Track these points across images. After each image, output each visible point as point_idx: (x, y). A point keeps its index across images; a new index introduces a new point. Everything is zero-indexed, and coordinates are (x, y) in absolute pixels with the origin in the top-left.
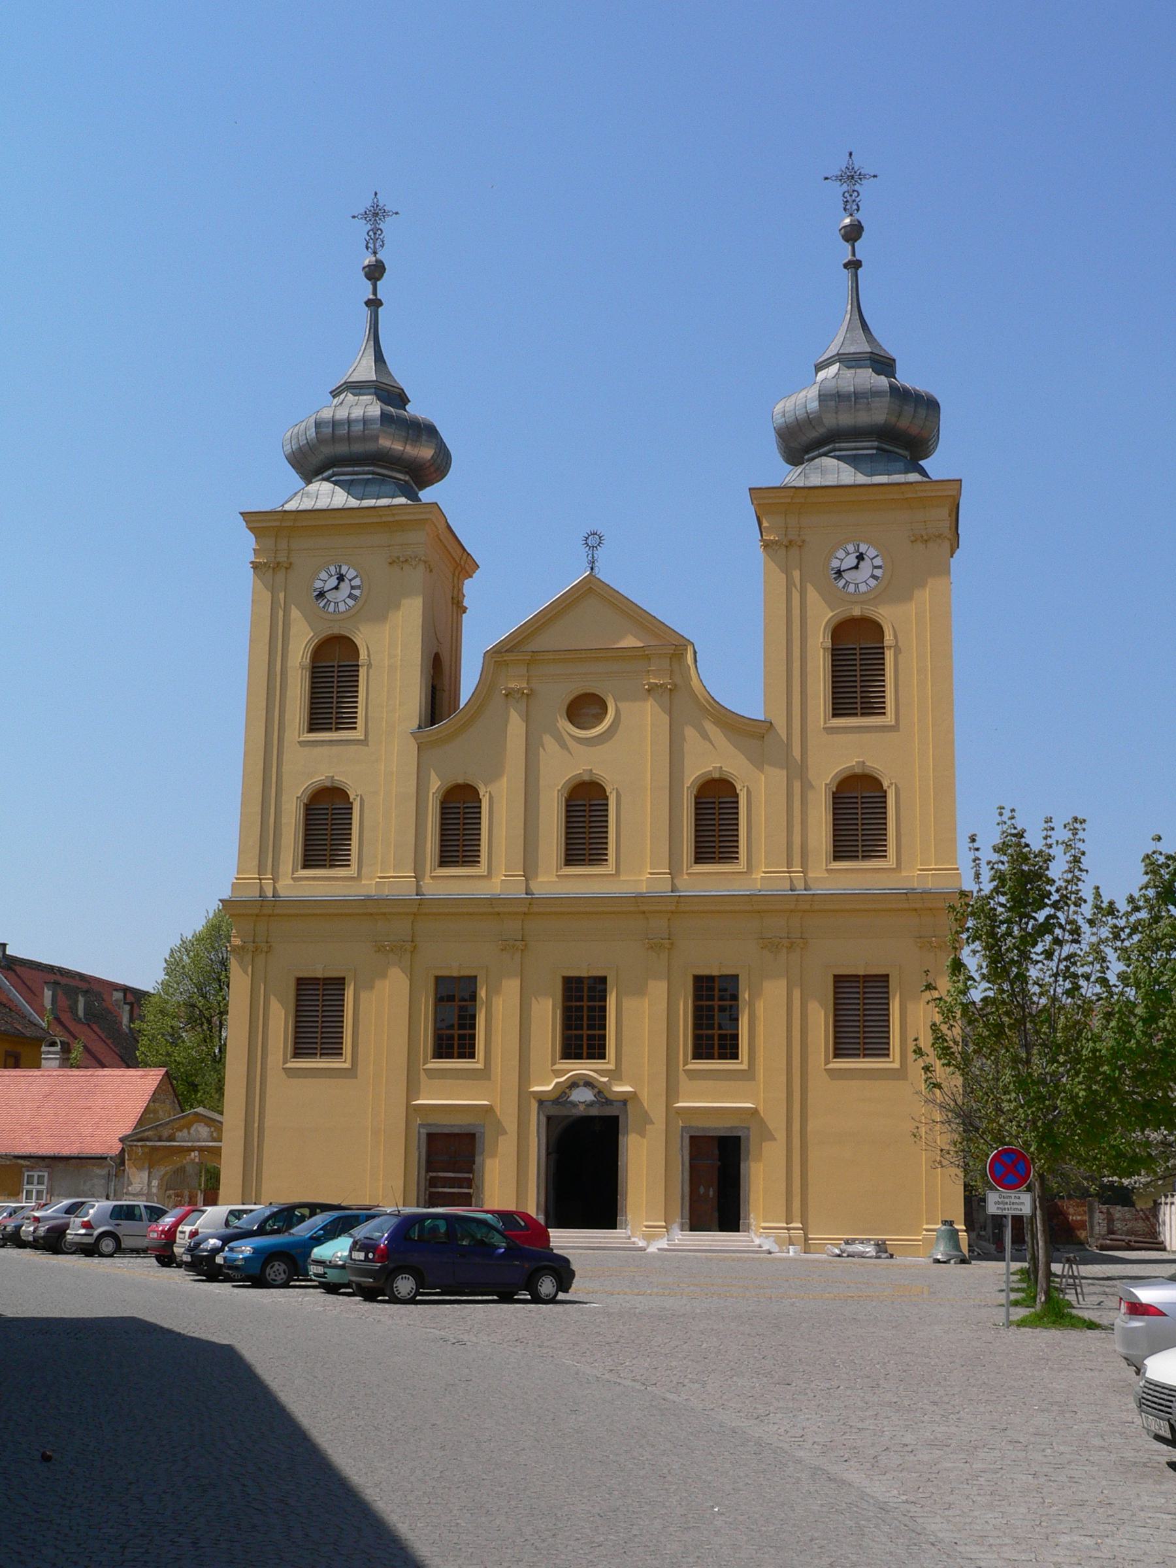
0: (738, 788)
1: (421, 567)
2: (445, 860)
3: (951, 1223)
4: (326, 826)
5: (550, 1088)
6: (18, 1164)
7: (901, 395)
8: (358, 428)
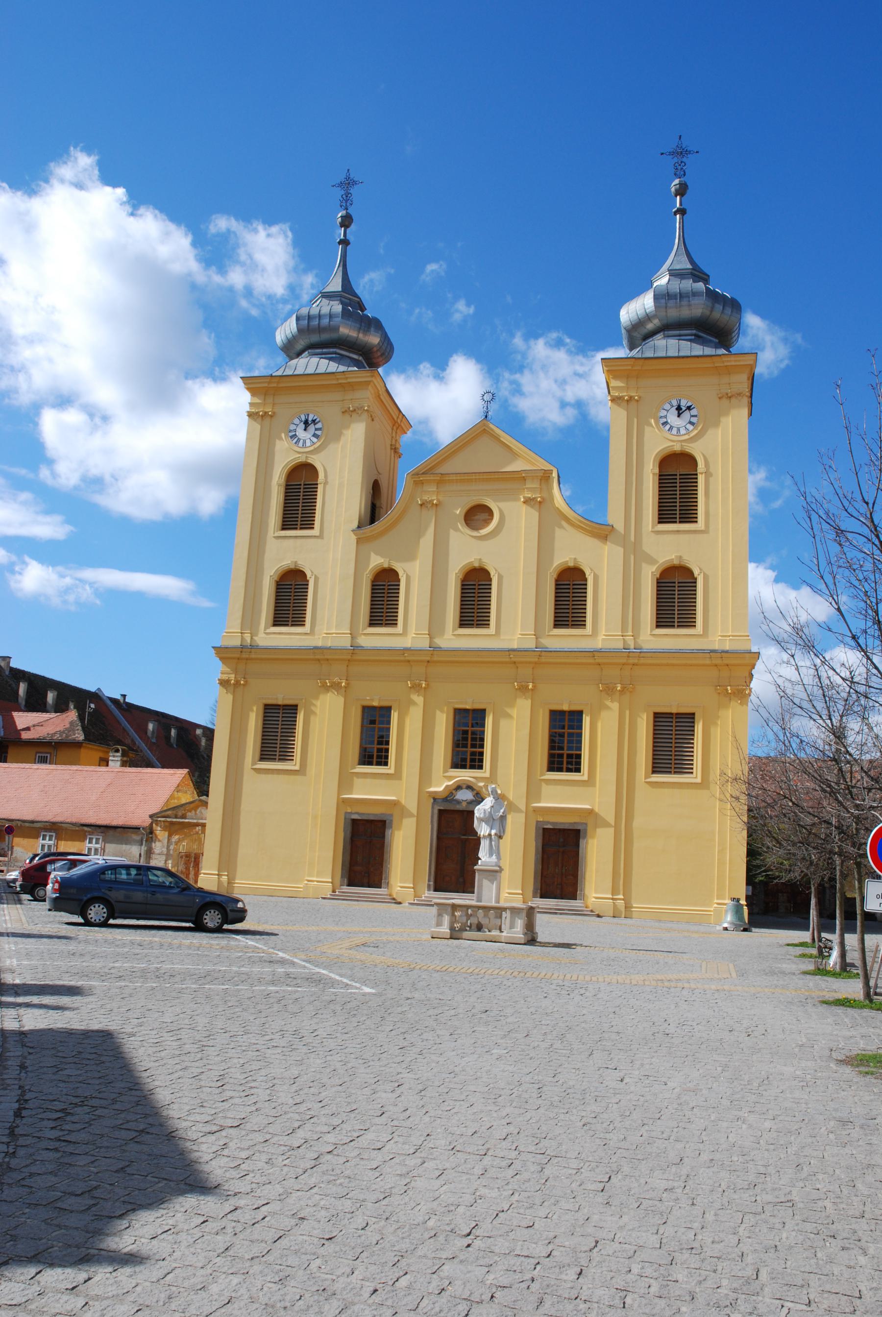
0: (587, 574)
1: (365, 416)
2: (559, 622)
3: (738, 900)
4: (290, 597)
5: (441, 789)
6: (83, 830)
7: (713, 296)
8: (325, 321)
